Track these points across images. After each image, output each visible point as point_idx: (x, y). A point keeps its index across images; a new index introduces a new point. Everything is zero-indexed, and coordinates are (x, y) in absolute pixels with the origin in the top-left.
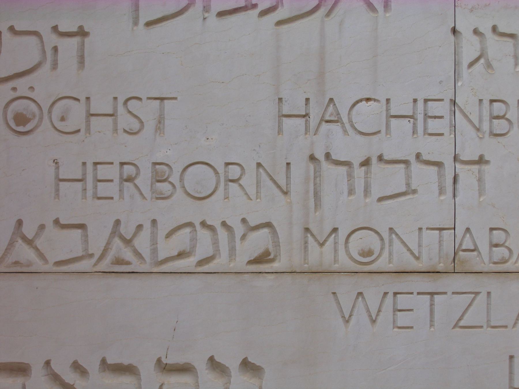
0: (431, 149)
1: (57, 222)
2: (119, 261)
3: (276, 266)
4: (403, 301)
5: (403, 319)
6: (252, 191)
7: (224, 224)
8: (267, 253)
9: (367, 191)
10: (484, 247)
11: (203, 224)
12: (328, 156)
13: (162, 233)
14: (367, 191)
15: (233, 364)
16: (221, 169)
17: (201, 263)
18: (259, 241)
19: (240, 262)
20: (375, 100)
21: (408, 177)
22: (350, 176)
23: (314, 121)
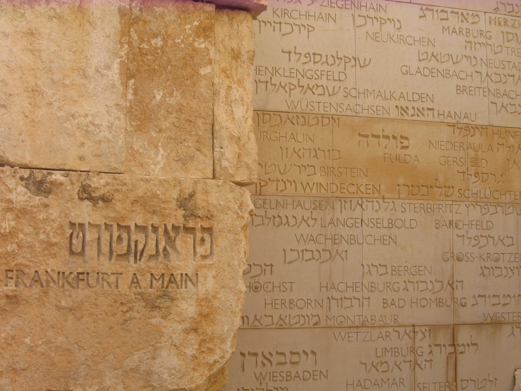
0: (359, 295)
1: (265, 315)
2: (281, 325)
3: (319, 326)
4: (350, 334)
5: (350, 339)
6: (314, 306)
7: (307, 315)
8: (317, 322)
9: (342, 307)
10: (370, 321)
11: (302, 315)
12: (332, 297)
13: (291, 317)
14: (342, 307)
15: (309, 352)
16: (306, 301)
17: (301, 325)
18: (316, 319)
19: (311, 325)
20: (256, 366)
21: (352, 302)
22: (338, 303)
23: (355, 385)
